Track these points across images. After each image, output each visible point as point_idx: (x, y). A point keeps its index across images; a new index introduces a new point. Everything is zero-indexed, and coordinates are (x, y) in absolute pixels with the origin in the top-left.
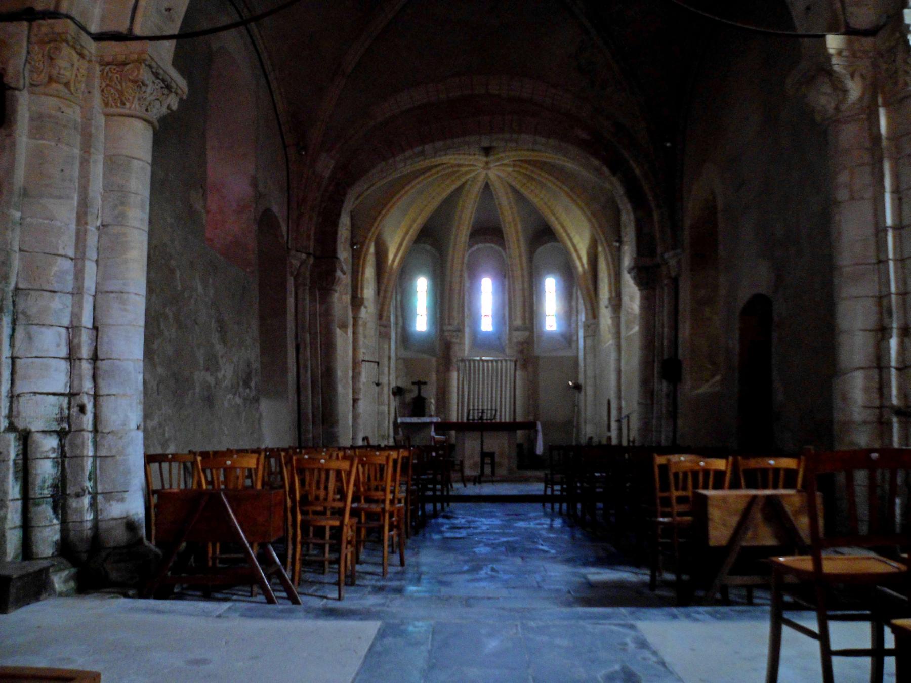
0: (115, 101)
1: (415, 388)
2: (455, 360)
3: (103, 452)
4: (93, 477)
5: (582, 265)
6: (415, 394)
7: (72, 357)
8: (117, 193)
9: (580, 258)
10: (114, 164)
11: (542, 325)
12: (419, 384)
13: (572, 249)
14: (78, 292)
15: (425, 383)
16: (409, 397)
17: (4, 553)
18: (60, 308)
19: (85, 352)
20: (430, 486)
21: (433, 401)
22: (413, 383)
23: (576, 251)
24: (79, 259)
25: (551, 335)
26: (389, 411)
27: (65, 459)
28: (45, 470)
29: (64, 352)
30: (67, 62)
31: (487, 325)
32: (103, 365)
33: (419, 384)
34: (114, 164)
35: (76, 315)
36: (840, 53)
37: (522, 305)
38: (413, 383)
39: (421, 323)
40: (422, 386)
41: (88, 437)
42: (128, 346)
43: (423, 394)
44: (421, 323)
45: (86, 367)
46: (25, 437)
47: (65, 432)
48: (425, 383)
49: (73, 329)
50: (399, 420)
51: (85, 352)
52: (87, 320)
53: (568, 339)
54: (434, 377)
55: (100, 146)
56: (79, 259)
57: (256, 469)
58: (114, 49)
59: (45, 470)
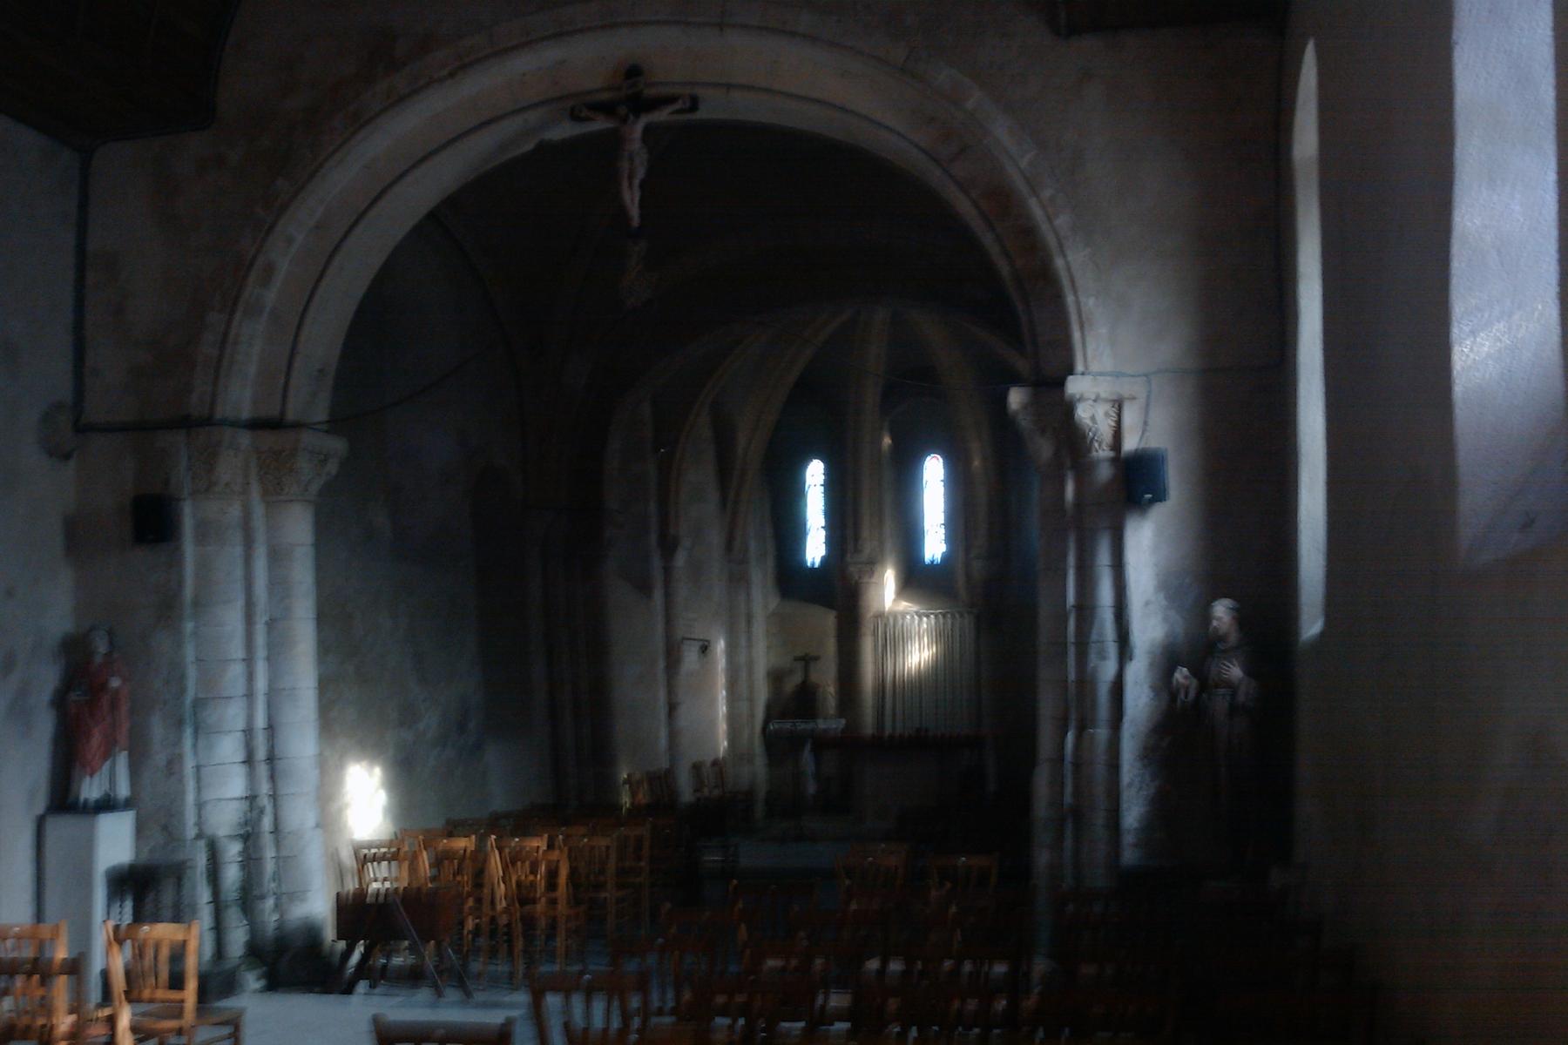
0: (274, 493)
1: (799, 665)
3: (284, 853)
4: (277, 877)
7: (249, 761)
8: (280, 586)
10: (277, 556)
12: (807, 661)
14: (250, 695)
15: (817, 659)
17: (1317, 46)
18: (233, 715)
19: (261, 754)
20: (720, 999)
22: (797, 659)
24: (249, 661)
27: (250, 862)
28: (232, 875)
29: (240, 756)
30: (228, 468)
31: (934, 470)
32: (280, 765)
34: (277, 556)
35: (250, 718)
36: (1025, 407)
43: (814, 677)
45: (262, 770)
47: (249, 836)
49: (249, 732)
51: (261, 754)
52: (260, 721)
53: (1215, 597)
56: (249, 661)
57: (1050, 220)
58: (269, 439)
59: (232, 875)
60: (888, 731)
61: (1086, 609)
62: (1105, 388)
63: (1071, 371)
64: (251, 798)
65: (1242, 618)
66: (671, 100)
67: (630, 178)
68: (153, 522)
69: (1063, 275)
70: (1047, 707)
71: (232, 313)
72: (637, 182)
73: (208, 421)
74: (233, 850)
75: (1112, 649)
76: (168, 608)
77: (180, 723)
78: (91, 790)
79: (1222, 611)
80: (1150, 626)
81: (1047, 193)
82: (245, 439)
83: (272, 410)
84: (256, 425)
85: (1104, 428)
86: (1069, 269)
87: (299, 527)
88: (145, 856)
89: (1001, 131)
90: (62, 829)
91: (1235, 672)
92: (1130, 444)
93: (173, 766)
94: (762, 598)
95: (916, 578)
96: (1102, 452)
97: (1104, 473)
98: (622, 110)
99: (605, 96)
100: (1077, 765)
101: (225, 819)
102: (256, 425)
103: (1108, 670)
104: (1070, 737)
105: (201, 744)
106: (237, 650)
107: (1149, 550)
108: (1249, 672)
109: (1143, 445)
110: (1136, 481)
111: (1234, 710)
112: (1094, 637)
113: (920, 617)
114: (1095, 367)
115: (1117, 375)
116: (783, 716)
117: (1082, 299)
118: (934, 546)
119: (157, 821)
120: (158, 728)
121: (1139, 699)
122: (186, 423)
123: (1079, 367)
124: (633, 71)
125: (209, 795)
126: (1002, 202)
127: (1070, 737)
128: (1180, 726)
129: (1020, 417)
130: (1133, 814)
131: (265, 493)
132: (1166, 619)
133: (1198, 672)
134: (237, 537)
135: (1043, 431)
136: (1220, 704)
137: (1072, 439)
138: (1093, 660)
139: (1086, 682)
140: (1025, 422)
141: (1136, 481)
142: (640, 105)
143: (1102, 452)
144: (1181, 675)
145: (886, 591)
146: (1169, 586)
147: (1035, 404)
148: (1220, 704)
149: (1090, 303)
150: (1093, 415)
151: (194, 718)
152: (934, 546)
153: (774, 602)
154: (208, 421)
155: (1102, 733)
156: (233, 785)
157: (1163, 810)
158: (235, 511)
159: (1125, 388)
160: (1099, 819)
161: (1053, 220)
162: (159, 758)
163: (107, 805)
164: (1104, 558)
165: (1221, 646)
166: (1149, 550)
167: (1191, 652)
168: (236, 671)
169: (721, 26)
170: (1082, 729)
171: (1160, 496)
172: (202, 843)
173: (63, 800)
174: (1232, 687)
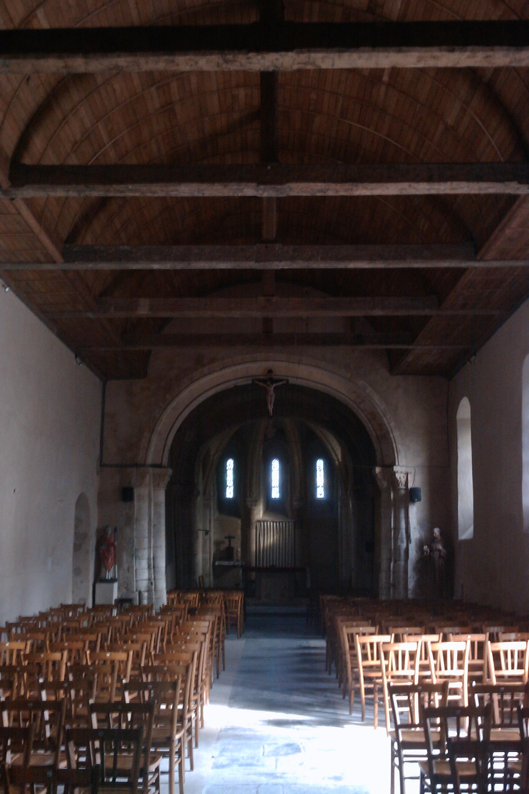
1: (227, 541)
2: (254, 521)
5: (338, 460)
6: (226, 545)
9: (337, 456)
11: (325, 464)
12: (230, 538)
13: (331, 450)
16: (223, 547)
18: (145, 553)
21: (239, 550)
22: (225, 538)
23: (334, 451)
25: (320, 500)
26: (210, 557)
31: (276, 465)
33: (230, 538)
36: (380, 473)
37: (298, 480)
38: (225, 538)
39: (230, 493)
40: (232, 540)
41: (154, 592)
42: (162, 563)
44: (230, 493)
46: (140, 593)
47: (149, 591)
48: (234, 538)
49: (149, 559)
50: (217, 563)
53: (434, 527)
54: (239, 532)
55: (152, 500)
58: (158, 470)
60: (268, 566)
61: (397, 529)
62: (404, 470)
63: (394, 464)
64: (149, 579)
65: (441, 534)
66: (282, 380)
67: (271, 403)
68: (127, 495)
69: (392, 438)
70: (384, 555)
71: (152, 434)
72: (272, 404)
73: (144, 465)
74: (146, 595)
75: (405, 541)
76: (130, 520)
77: (133, 556)
78: (109, 575)
79: (436, 531)
80: (416, 534)
81: (388, 417)
82: (151, 470)
83: (158, 462)
84: (154, 466)
85: (403, 480)
86: (394, 437)
87: (162, 497)
88: (120, 597)
89: (376, 398)
90: (100, 587)
91: (440, 547)
92: (410, 485)
93: (130, 569)
94: (214, 514)
95: (272, 507)
96: (402, 487)
97: (403, 492)
98: (269, 383)
99: (261, 377)
100: (394, 572)
101: (143, 585)
102: (154, 466)
103: (404, 545)
104: (392, 564)
105: (137, 562)
106: (146, 534)
107: (415, 513)
108: (444, 547)
109: (413, 487)
110: (412, 495)
111: (440, 556)
112: (399, 537)
113: (273, 522)
114: (401, 464)
115: (407, 467)
116: (220, 559)
117: (397, 445)
118: (275, 494)
119: (127, 585)
120: (125, 558)
121: (413, 553)
122: (137, 465)
123: (397, 464)
124: (270, 371)
125: (138, 578)
126: (374, 416)
127: (392, 564)
128: (424, 561)
129: (378, 475)
130: (411, 584)
131: (154, 486)
132: (419, 532)
133: (430, 547)
134: (147, 499)
135: (384, 480)
136: (436, 554)
137: (393, 481)
138: (399, 543)
139: (397, 548)
140: (379, 476)
141: (412, 495)
142: (273, 381)
143: (402, 487)
144: (425, 547)
145: (259, 513)
146: (421, 524)
147: (382, 472)
148: (436, 554)
149: (399, 447)
150: (400, 476)
151: (134, 555)
152: (275, 494)
153: (217, 514)
154: (144, 465)
155: (402, 563)
156: (144, 575)
157: (419, 584)
158: (146, 492)
159: (409, 470)
160: (401, 586)
161: (390, 424)
162: (125, 566)
163: (113, 580)
164: (402, 515)
165: (436, 540)
166: (415, 513)
167: (428, 540)
168: (146, 540)
169: (299, 363)
170: (395, 562)
171: (419, 500)
172: (137, 593)
173: (99, 578)
174: (440, 551)
